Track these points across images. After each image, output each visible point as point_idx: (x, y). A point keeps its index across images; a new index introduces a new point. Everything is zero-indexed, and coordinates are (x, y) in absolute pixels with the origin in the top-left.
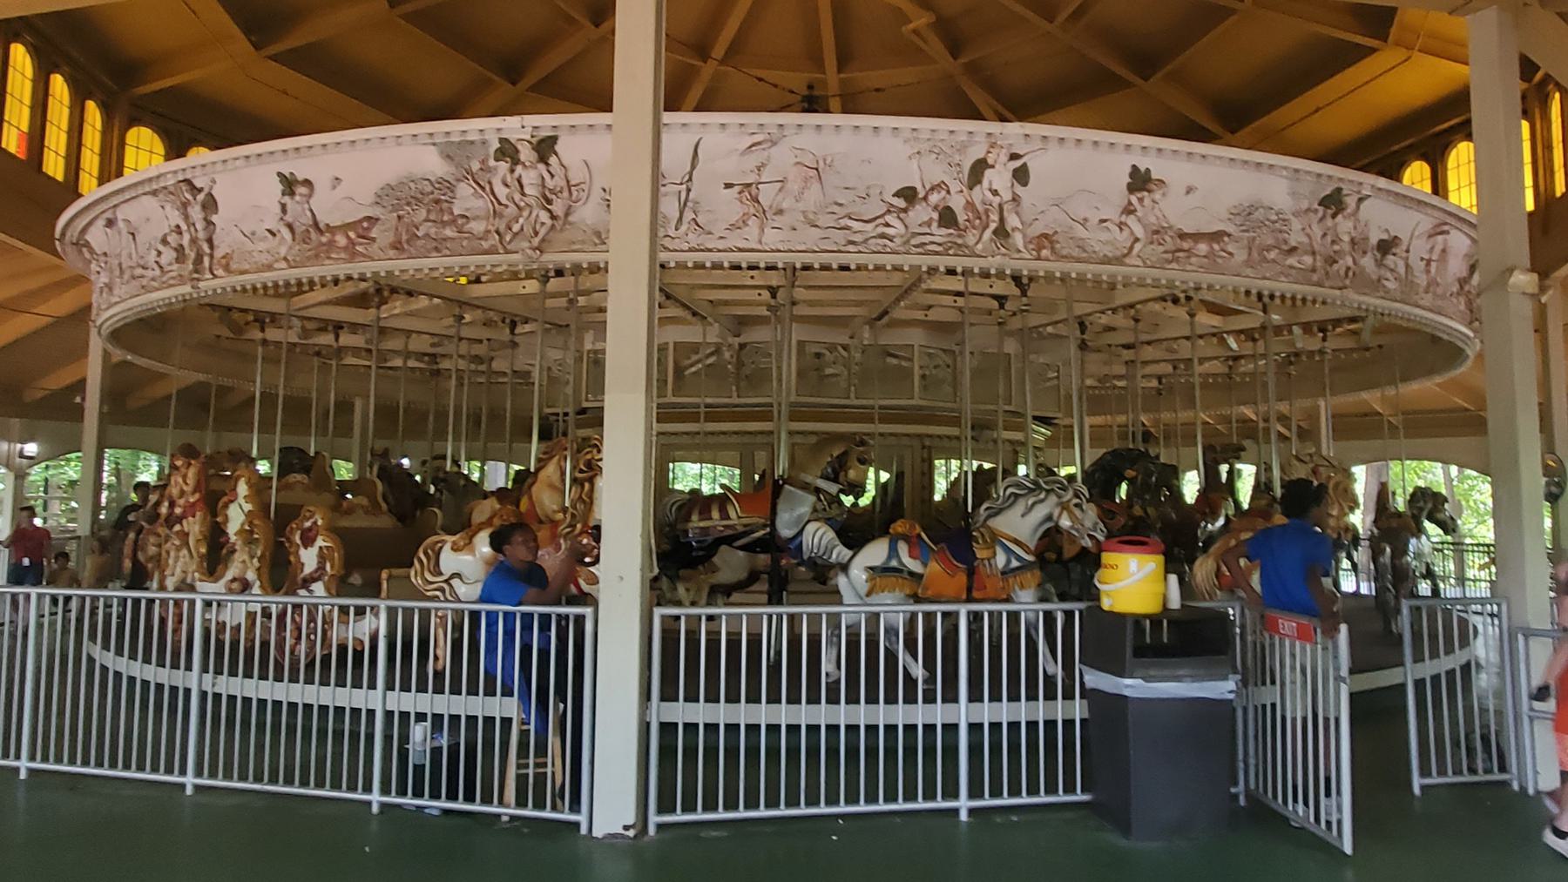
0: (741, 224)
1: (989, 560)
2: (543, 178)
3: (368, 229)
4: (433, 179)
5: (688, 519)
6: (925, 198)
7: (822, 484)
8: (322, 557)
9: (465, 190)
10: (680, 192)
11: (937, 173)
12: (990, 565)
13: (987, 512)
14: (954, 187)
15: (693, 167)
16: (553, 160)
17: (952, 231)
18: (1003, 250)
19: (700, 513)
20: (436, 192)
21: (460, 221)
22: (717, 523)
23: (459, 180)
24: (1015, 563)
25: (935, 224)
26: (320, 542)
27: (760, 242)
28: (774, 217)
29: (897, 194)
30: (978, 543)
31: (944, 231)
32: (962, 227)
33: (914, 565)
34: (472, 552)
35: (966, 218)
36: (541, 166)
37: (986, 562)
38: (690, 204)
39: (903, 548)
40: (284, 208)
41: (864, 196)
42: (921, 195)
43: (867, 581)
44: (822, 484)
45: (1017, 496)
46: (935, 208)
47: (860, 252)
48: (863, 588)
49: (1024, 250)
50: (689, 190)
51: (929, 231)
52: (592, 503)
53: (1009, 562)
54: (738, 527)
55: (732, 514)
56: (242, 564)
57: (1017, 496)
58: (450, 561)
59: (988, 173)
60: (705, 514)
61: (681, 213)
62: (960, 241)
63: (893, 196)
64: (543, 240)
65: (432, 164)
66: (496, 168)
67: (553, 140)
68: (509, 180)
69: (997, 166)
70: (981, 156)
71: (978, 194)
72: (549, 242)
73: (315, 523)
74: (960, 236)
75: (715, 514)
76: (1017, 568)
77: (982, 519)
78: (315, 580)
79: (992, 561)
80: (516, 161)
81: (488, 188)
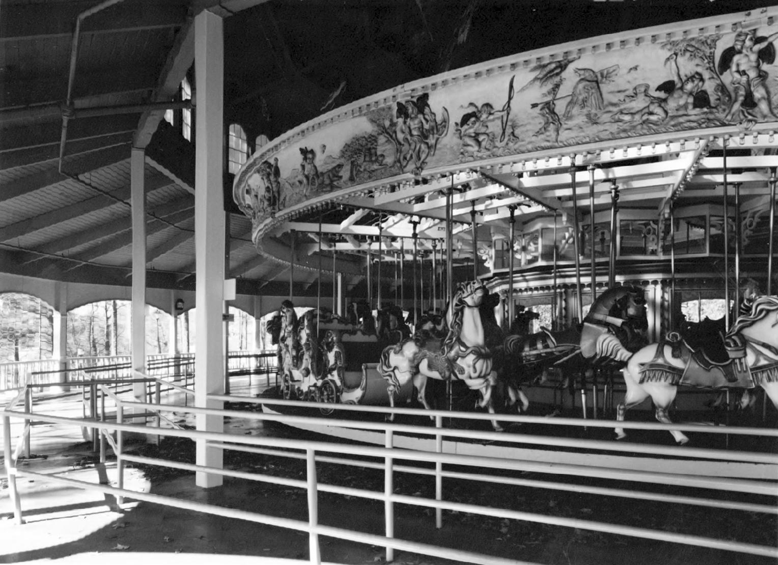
0: (543, 130)
1: (740, 359)
2: (422, 123)
3: (338, 172)
4: (366, 136)
5: (522, 349)
6: (682, 88)
7: (611, 319)
8: (337, 356)
9: (382, 139)
10: (502, 116)
11: (688, 66)
12: (741, 364)
13: (741, 324)
14: (706, 75)
15: (510, 98)
16: (427, 110)
17: (705, 110)
18: (750, 117)
19: (530, 347)
20: (369, 144)
21: (380, 159)
22: (542, 351)
23: (379, 134)
24: (763, 362)
25: (690, 107)
26: (336, 349)
27: (557, 141)
28: (566, 122)
29: (659, 89)
30: (730, 346)
31: (698, 110)
32: (713, 105)
33: (677, 363)
34: (402, 354)
35: (717, 97)
36: (421, 116)
37: (737, 361)
38: (509, 123)
39: (668, 351)
40: (303, 167)
41: (633, 95)
42: (679, 85)
43: (639, 373)
44: (611, 319)
45: (768, 312)
46: (691, 94)
47: (629, 137)
48: (638, 377)
49: (770, 115)
50: (508, 114)
51: (686, 113)
52: (462, 323)
53: (757, 361)
54: (555, 353)
55: (551, 345)
56: (307, 362)
57: (768, 312)
58: (394, 359)
59: (736, 58)
60: (533, 346)
61: (504, 130)
62: (711, 117)
63: (656, 90)
64: (423, 162)
65: (364, 126)
66: (397, 123)
67: (426, 96)
68: (404, 128)
69: (744, 51)
70: (730, 45)
71: (727, 78)
72: (426, 163)
73: (332, 339)
74: (711, 113)
75: (540, 346)
76: (764, 366)
77: (736, 329)
78: (334, 369)
79: (743, 360)
80: (407, 116)
81: (394, 136)
